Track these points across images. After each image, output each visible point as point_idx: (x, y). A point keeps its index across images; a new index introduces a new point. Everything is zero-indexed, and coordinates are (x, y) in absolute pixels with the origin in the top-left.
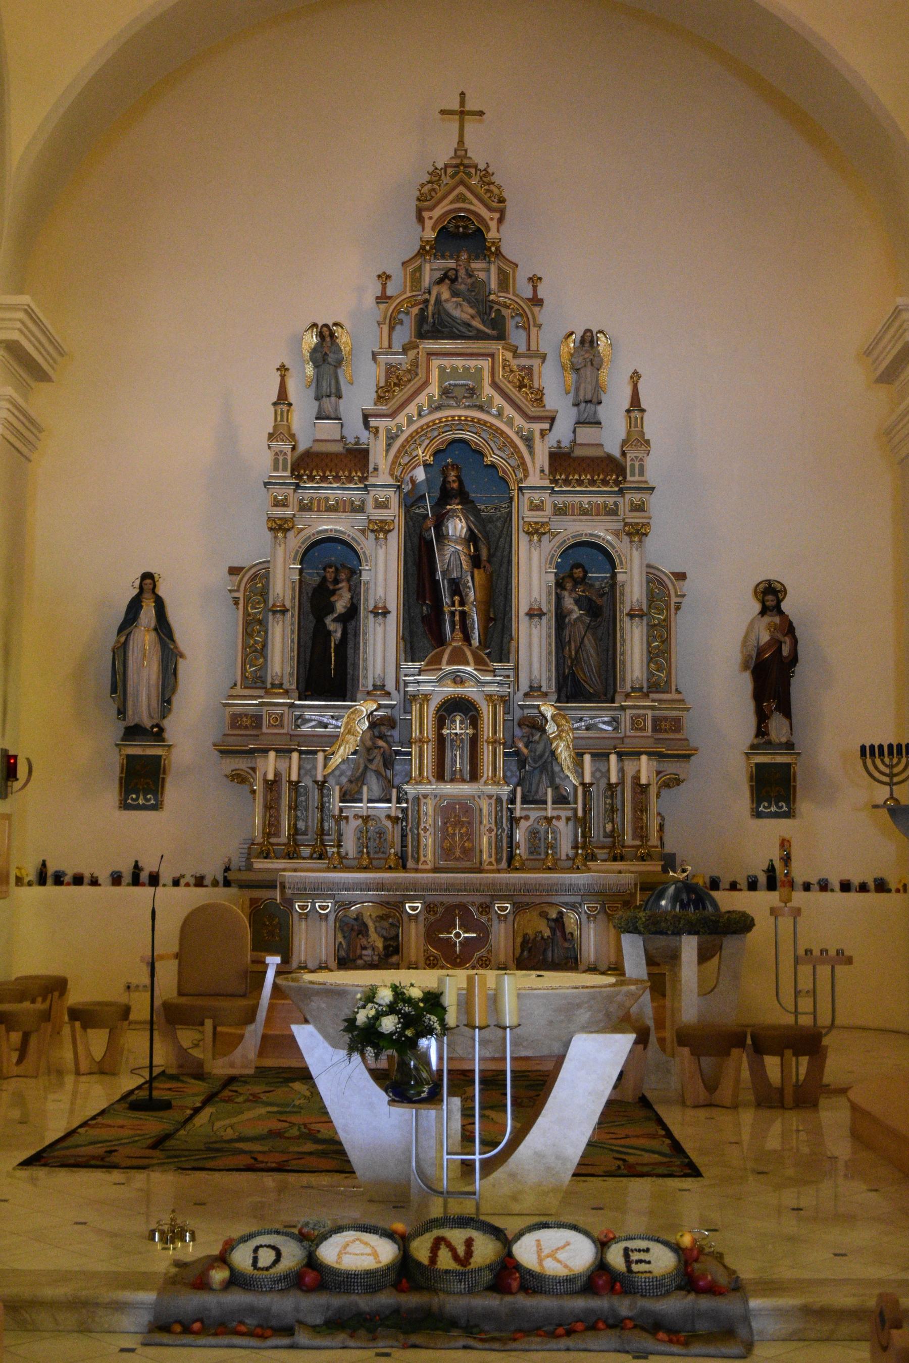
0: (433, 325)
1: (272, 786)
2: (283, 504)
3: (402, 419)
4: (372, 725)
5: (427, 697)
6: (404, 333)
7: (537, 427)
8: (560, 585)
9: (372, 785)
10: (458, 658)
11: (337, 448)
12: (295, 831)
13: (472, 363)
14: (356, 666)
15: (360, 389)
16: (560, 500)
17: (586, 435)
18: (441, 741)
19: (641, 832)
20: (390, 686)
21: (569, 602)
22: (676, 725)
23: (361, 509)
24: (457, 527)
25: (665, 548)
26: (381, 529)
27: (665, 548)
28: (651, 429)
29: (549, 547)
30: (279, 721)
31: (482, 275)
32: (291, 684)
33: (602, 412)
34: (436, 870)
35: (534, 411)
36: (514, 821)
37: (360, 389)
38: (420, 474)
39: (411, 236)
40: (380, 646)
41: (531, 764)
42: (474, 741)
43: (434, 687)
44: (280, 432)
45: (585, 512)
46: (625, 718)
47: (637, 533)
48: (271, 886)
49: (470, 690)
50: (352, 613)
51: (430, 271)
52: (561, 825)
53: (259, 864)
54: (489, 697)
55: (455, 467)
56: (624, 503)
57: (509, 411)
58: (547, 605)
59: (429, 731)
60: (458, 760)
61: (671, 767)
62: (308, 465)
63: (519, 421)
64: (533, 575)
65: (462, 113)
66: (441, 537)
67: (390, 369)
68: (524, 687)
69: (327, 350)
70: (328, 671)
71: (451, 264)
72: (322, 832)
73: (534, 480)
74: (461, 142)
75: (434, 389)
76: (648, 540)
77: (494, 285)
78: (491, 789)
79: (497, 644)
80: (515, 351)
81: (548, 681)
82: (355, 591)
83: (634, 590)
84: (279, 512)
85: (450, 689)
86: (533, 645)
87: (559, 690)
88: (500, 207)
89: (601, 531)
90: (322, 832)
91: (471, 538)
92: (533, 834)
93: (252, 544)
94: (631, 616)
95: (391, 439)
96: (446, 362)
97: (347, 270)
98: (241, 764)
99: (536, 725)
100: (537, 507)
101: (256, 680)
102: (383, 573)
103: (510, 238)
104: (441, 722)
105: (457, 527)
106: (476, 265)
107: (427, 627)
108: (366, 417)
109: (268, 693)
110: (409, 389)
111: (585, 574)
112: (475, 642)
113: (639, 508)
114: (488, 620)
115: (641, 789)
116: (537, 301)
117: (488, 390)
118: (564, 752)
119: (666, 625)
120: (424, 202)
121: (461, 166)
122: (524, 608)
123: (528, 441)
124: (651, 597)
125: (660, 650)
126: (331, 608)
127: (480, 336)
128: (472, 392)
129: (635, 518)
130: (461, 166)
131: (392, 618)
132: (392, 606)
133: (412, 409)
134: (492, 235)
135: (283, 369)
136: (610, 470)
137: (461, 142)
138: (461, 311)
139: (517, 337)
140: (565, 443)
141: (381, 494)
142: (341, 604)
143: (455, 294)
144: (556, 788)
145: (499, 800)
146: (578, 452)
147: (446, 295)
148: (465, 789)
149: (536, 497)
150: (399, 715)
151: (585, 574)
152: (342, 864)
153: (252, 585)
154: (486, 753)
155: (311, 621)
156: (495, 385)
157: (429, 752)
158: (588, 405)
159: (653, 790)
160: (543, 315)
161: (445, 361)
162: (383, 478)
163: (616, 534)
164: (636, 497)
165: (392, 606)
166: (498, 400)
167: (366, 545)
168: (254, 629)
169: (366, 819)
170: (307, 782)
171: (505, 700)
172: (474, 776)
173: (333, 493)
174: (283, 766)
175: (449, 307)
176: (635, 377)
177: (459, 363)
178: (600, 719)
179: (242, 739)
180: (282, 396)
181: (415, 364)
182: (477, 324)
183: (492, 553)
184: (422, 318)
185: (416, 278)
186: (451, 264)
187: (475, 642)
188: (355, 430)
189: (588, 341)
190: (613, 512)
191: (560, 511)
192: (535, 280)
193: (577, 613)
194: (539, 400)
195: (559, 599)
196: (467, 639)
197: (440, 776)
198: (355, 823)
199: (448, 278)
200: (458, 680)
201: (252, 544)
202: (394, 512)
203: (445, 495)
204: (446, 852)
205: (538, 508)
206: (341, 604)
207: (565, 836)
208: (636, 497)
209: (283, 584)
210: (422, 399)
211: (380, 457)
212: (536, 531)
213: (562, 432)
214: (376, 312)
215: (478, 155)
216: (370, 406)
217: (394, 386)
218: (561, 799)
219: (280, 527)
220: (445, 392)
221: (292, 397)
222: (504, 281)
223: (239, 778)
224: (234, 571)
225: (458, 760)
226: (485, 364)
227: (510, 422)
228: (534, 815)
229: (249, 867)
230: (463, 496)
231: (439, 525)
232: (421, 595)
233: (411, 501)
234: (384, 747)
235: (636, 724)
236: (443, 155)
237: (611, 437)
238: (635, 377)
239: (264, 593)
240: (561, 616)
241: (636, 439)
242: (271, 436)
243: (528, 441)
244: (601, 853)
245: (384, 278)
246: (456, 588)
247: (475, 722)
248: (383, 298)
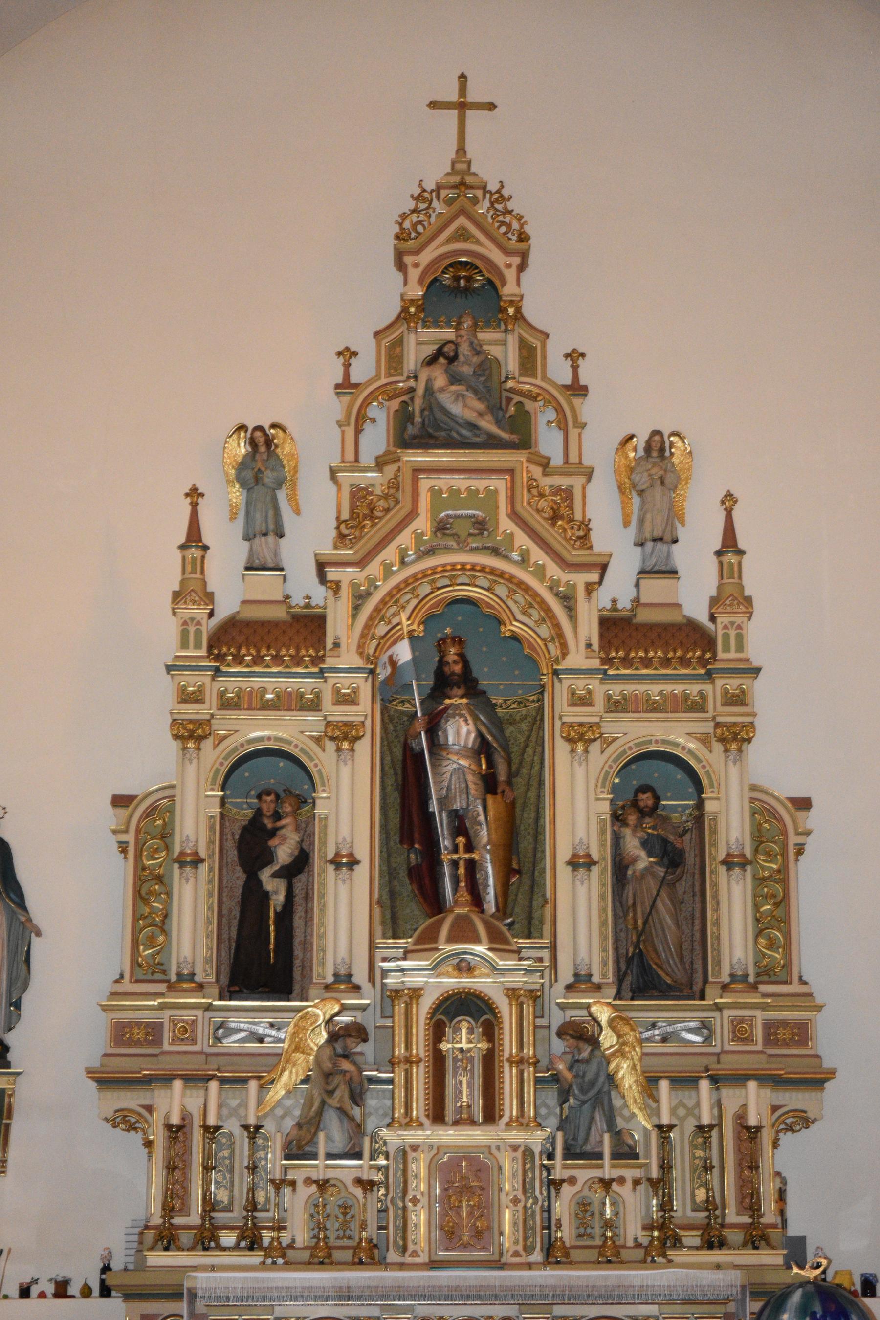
0: (420, 428)
1: (176, 1132)
2: (196, 698)
3: (374, 568)
4: (333, 1037)
5: (416, 993)
6: (376, 438)
7: (580, 579)
8: (617, 817)
9: (333, 1133)
10: (463, 932)
11: (280, 613)
12: (210, 1206)
13: (480, 484)
14: (307, 945)
15: (312, 523)
16: (616, 689)
17: (655, 590)
18: (438, 1060)
19: (750, 1201)
20: (360, 976)
21: (632, 844)
22: (801, 1033)
23: (314, 705)
24: (460, 732)
25: (777, 761)
26: (344, 735)
27: (777, 761)
28: (754, 579)
29: (600, 760)
30: (187, 1032)
31: (495, 351)
32: (205, 973)
33: (680, 556)
34: (434, 1264)
35: (575, 555)
36: (554, 1185)
37: (312, 523)
38: (404, 652)
39: (387, 292)
40: (343, 915)
41: (581, 1090)
42: (489, 1060)
43: (425, 977)
44: (192, 590)
45: (654, 707)
46: (722, 1022)
47: (735, 737)
48: (176, 1295)
49: (482, 983)
50: (301, 862)
51: (419, 343)
52: (625, 1191)
53: (158, 1258)
54: (512, 993)
55: (458, 640)
56: (714, 691)
57: (538, 556)
58: (598, 848)
59: (420, 1048)
60: (464, 1090)
61: (793, 1099)
62: (236, 639)
63: (553, 570)
64: (577, 805)
65: (462, 106)
66: (437, 746)
67: (359, 494)
68: (566, 975)
69: (262, 458)
70: (263, 956)
71: (448, 334)
72: (252, 1206)
73: (576, 658)
74: (461, 150)
75: (422, 524)
76: (752, 749)
77: (512, 364)
78: (517, 1136)
79: (521, 912)
80: (545, 464)
81: (601, 968)
82: (306, 829)
83: (732, 827)
84: (190, 711)
85: (451, 982)
86: (580, 912)
87: (620, 980)
88: (520, 246)
89: (679, 735)
90: (252, 1206)
91: (483, 748)
92: (583, 1207)
93: (150, 760)
94: (728, 863)
95: (360, 598)
96: (442, 482)
97: (302, 327)
98: (131, 1100)
99: (581, 1034)
100: (583, 701)
101: (149, 967)
102: (349, 804)
103: (540, 293)
104: (438, 1033)
105: (460, 732)
106: (485, 335)
107: (420, 878)
108: (321, 567)
109: (172, 988)
110: (386, 524)
111: (657, 807)
112: (490, 905)
113: (738, 699)
114: (508, 871)
115: (749, 1134)
116: (577, 389)
117: (506, 524)
118: (626, 1074)
119: (783, 876)
120: (407, 243)
121: (462, 184)
122: (564, 854)
123: (568, 600)
124: (759, 839)
125: (775, 915)
126: (268, 858)
127: (492, 443)
128: (481, 526)
129: (731, 716)
130: (462, 184)
131: (362, 872)
132: (362, 852)
133: (390, 553)
134: (508, 290)
135: (194, 494)
136: (688, 643)
137: (461, 150)
138: (463, 407)
139: (549, 441)
140: (625, 603)
141: (345, 682)
142: (284, 853)
143: (454, 379)
144: (618, 1135)
145: (528, 1153)
146: (644, 616)
147: (440, 381)
148: (477, 1136)
149: (580, 684)
150: (371, 1021)
151: (657, 807)
152: (280, 1255)
153: (145, 824)
154: (508, 1076)
155: (239, 877)
156: (514, 516)
157: (420, 1076)
158: (658, 542)
159: (767, 1136)
160: (587, 409)
161: (446, 478)
162: (349, 658)
163: (704, 740)
164: (732, 684)
165: (362, 852)
166: (522, 540)
167: (324, 760)
168: (149, 893)
169: (323, 1185)
170: (232, 1126)
171: (535, 996)
172: (491, 1116)
173: (271, 682)
174: (194, 1103)
175: (446, 399)
176: (729, 501)
177: (461, 482)
178: (682, 1025)
179: (130, 1066)
180: (194, 535)
181: (395, 485)
182: (487, 424)
183: (511, 772)
184: (403, 417)
185: (393, 357)
186: (448, 334)
187: (490, 905)
188: (303, 587)
189: (657, 447)
190: (698, 706)
191: (616, 706)
192: (574, 357)
193: (644, 861)
194: (584, 539)
195: (617, 840)
196: (477, 901)
197: (438, 1116)
198: (306, 1192)
199: (444, 356)
200: (464, 968)
201: (150, 760)
202: (364, 710)
203: (442, 684)
204: (450, 1234)
205: (583, 701)
206: (284, 853)
207: (634, 1210)
208: (732, 684)
209: (196, 820)
210: (405, 538)
211: (340, 625)
212: (581, 736)
213: (619, 588)
214: (335, 407)
215: (487, 169)
216: (327, 550)
217: (361, 518)
218: (625, 1153)
219: (190, 734)
220: (441, 527)
221: (207, 538)
222: (529, 358)
223: (124, 1121)
224: (120, 801)
225: (464, 1090)
226: (499, 484)
227: (540, 572)
228: (584, 1175)
229: (141, 1266)
230: (469, 683)
231: (433, 728)
232: (406, 837)
233: (389, 691)
234: (342, 1075)
235: (740, 1032)
236: (435, 170)
237: (693, 594)
238: (729, 501)
239: (166, 835)
240: (620, 867)
241: (732, 597)
242: (177, 596)
243: (568, 600)
244: (692, 1238)
245: (348, 354)
246: (461, 826)
247: (490, 1031)
248: (345, 386)
